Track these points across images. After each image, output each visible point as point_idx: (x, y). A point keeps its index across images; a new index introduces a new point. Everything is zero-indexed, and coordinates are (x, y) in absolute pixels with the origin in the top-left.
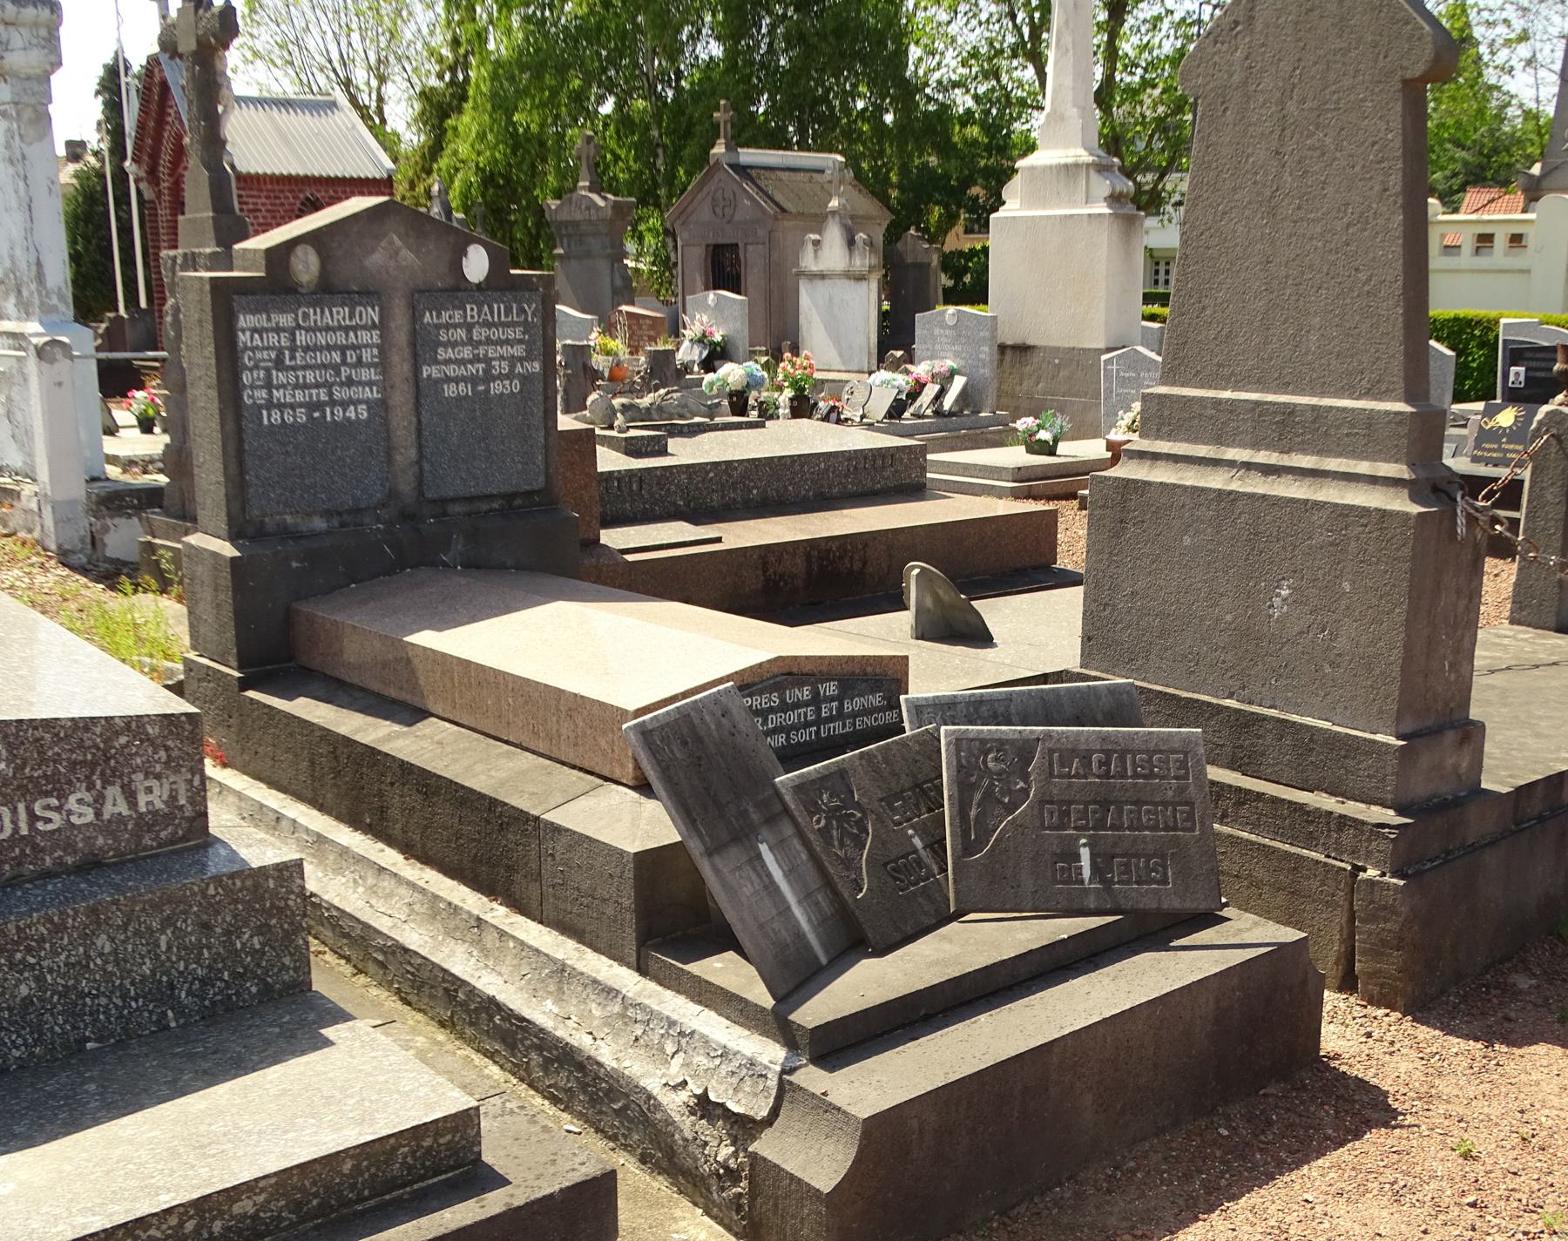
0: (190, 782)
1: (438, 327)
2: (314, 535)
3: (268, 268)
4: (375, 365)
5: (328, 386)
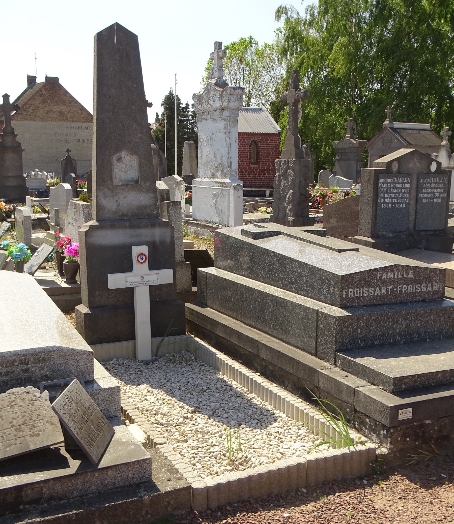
0: (442, 285)
1: (424, 183)
2: (389, 238)
3: (387, 167)
5: (397, 198)
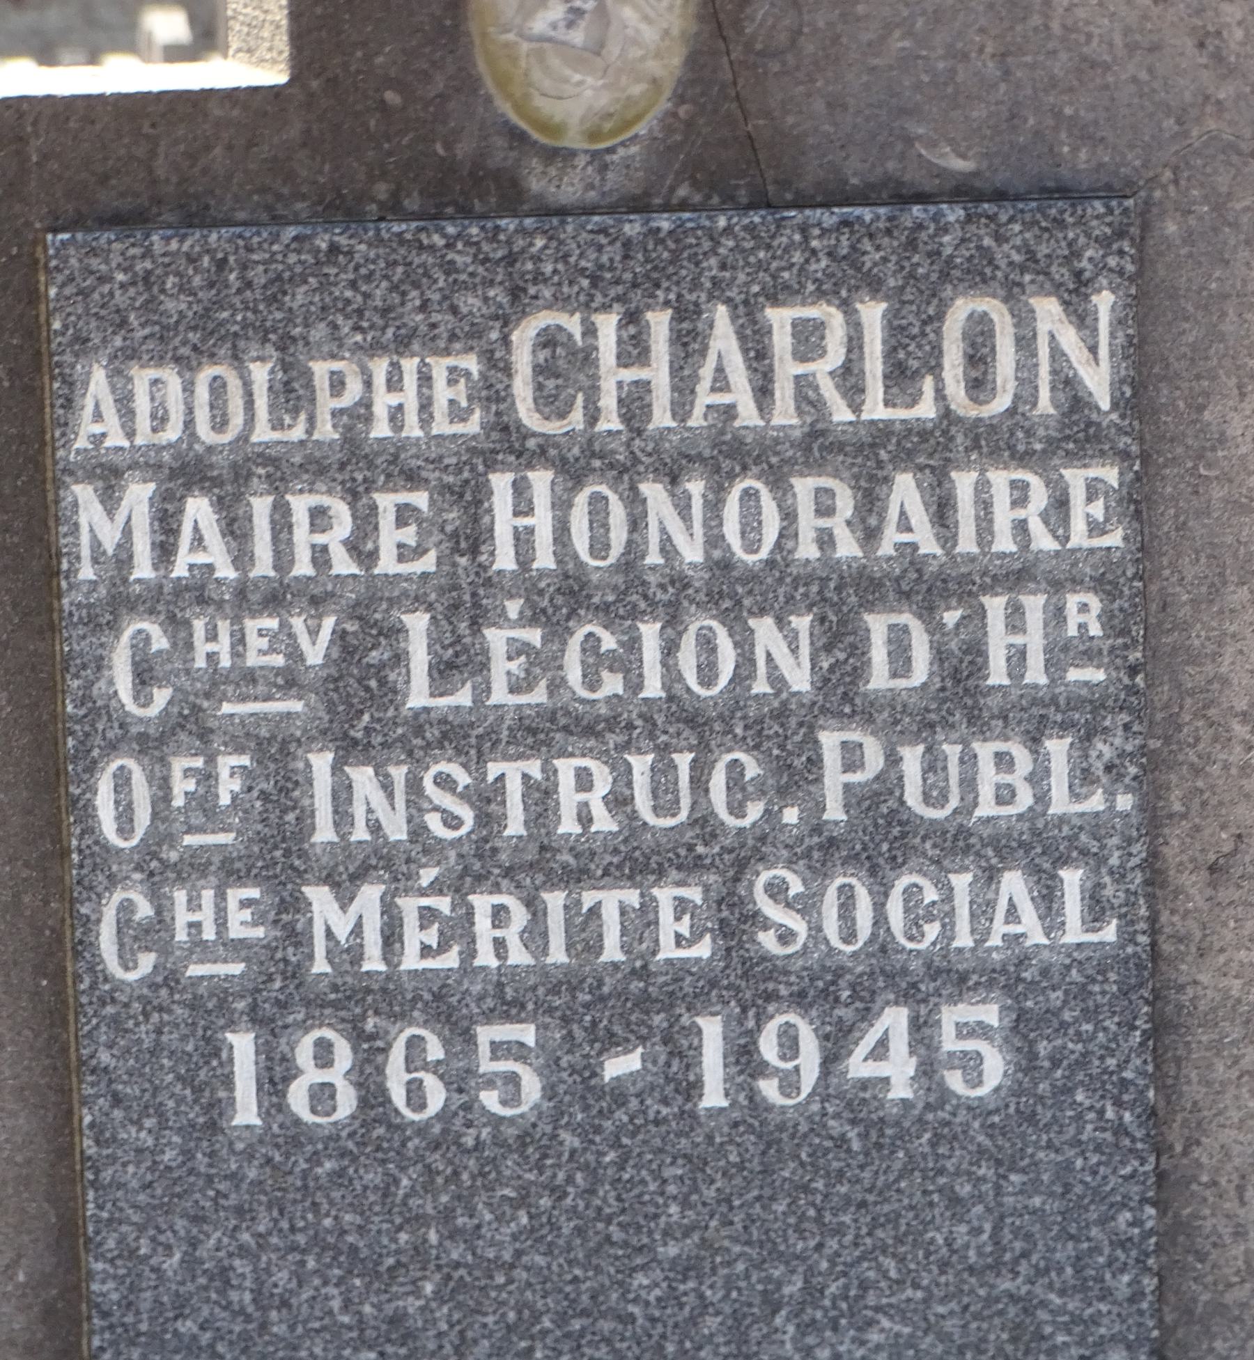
4: (1081, 717)
